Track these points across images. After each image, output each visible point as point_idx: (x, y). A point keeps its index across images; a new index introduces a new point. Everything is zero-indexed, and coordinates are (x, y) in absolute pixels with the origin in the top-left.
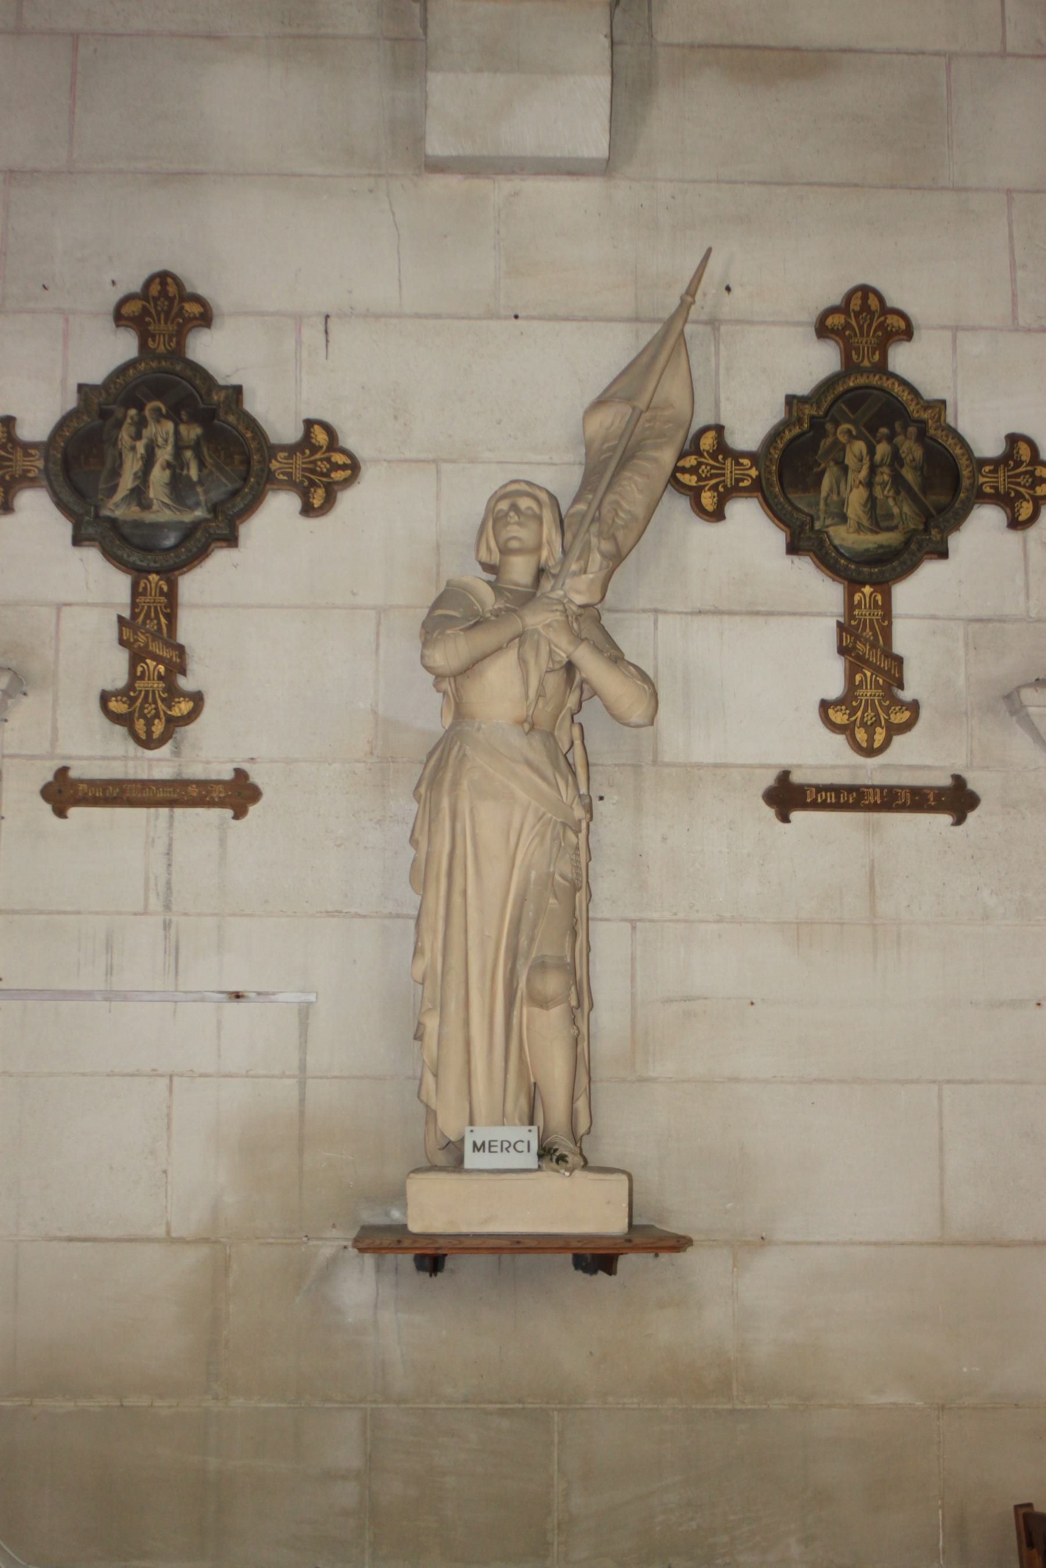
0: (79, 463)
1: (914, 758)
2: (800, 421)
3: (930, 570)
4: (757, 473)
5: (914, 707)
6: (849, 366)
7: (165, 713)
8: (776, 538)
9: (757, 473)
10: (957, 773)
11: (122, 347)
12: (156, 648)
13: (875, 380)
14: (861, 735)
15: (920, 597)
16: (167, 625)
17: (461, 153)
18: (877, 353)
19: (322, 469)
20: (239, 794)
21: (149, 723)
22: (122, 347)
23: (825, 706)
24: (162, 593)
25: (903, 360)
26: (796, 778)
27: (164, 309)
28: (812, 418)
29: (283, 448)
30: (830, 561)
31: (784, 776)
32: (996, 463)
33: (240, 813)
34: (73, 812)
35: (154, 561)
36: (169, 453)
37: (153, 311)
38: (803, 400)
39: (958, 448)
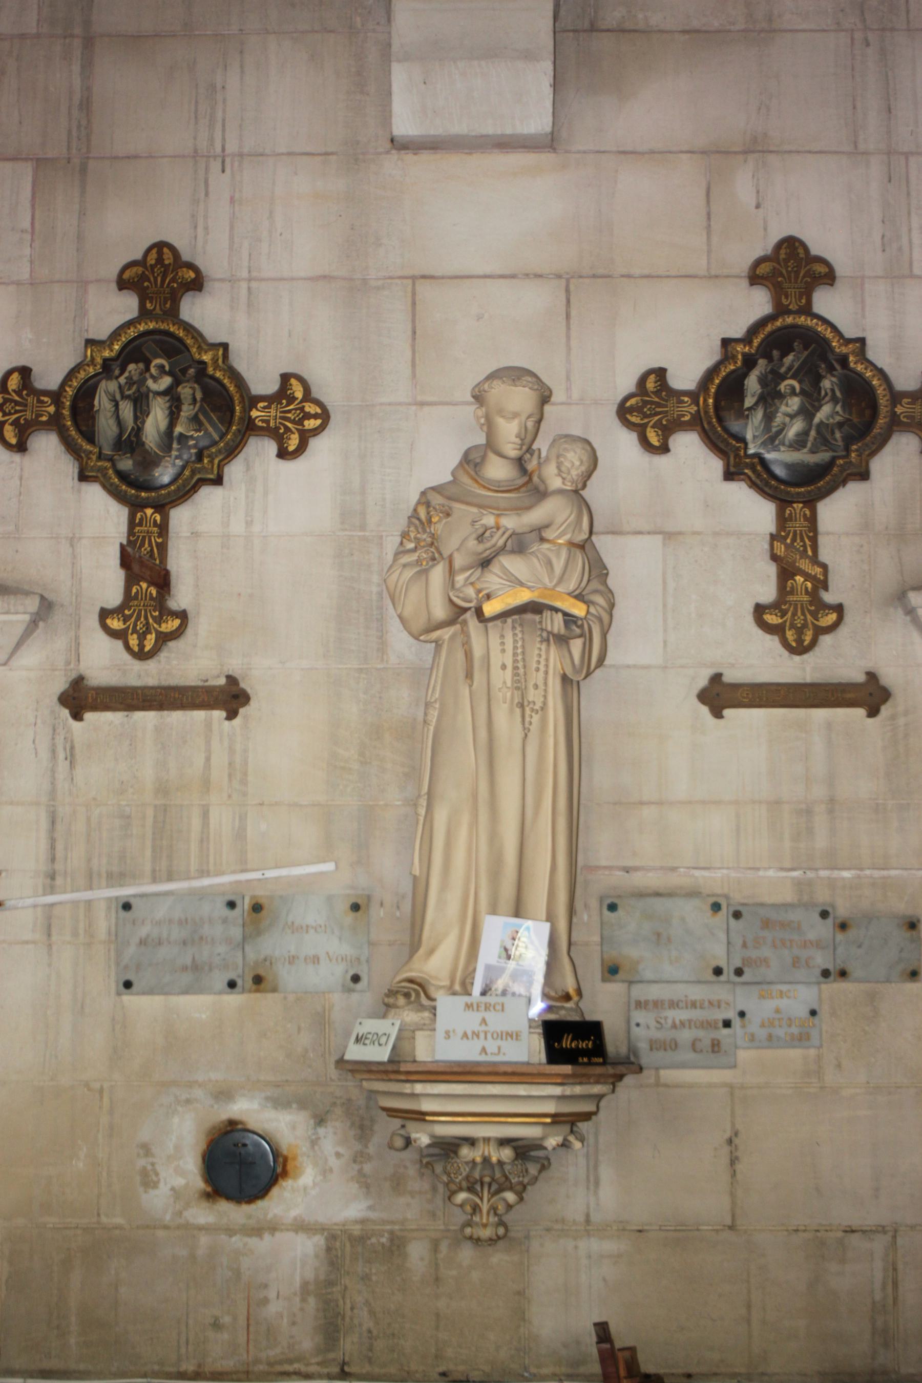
0: (72, 413)
1: (836, 658)
2: (734, 357)
4: (252, 413)
5: (839, 609)
6: (780, 310)
7: (813, 623)
9: (252, 413)
10: (230, 673)
11: (758, 304)
12: (804, 565)
13: (802, 320)
14: (310, 424)
15: (838, 512)
16: (159, 553)
19: (294, 417)
20: (231, 698)
22: (758, 304)
23: (759, 610)
26: (728, 678)
27: (162, 277)
28: (744, 355)
29: (262, 398)
30: (761, 478)
31: (716, 678)
32: (271, 399)
33: (232, 715)
34: (89, 716)
35: (146, 494)
36: (161, 404)
37: (784, 272)
39: (876, 379)
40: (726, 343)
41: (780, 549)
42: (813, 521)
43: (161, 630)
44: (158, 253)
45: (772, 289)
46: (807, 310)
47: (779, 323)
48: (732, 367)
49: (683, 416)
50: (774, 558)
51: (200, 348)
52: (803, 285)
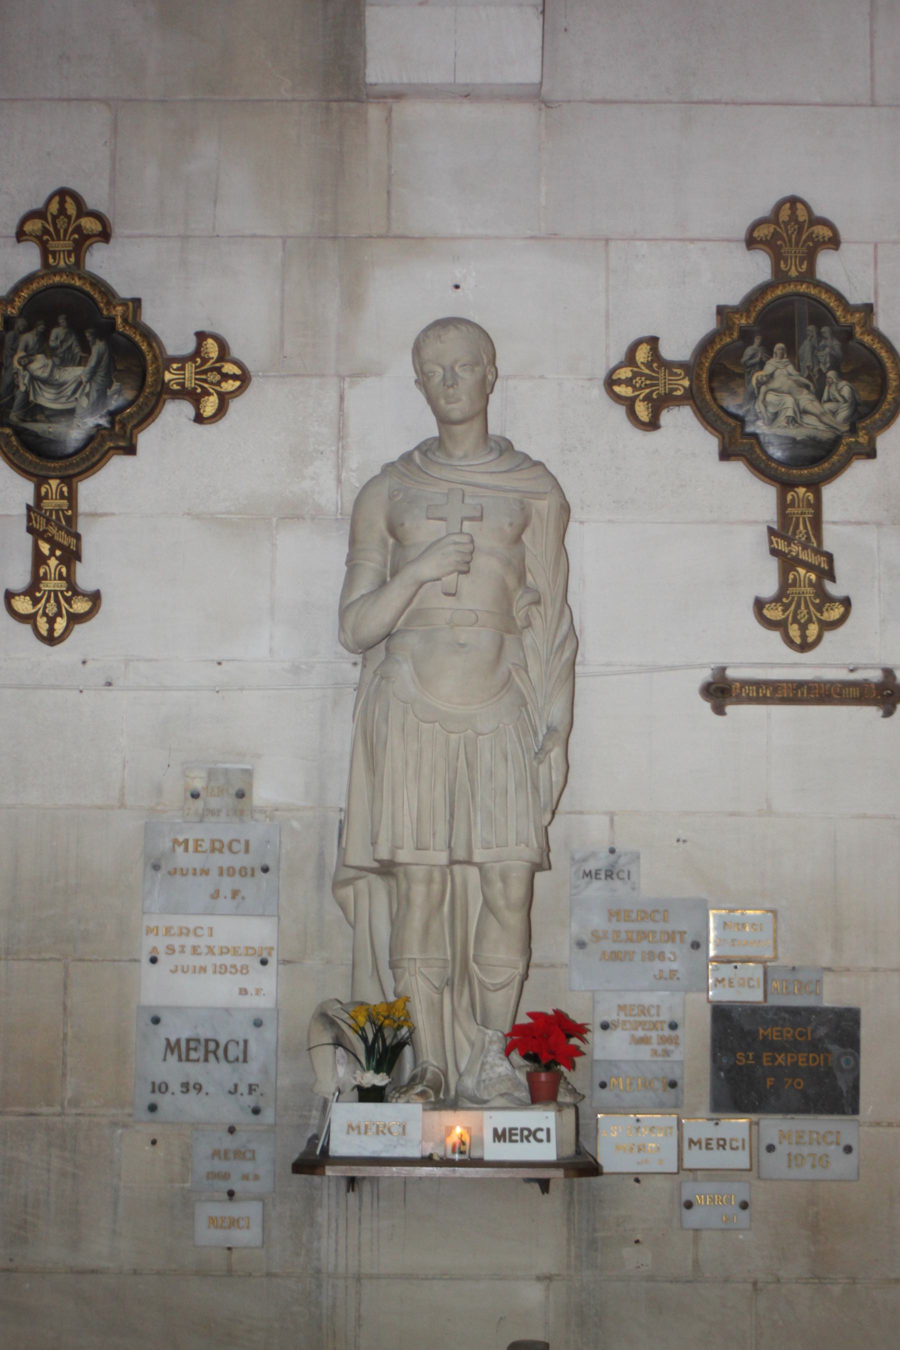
3: (859, 469)
6: (779, 276)
8: (708, 443)
11: (757, 269)
13: (803, 288)
14: (794, 631)
17: (396, 80)
18: (805, 263)
21: (803, 628)
22: (757, 269)
24: (809, 505)
25: (829, 268)
29: (174, 360)
30: (762, 467)
38: (736, 310)
40: (721, 311)
41: (781, 546)
42: (817, 506)
43: (823, 618)
44: (791, 208)
45: (769, 251)
46: (809, 276)
47: (779, 292)
48: (728, 340)
49: (676, 389)
50: (774, 552)
51: (109, 304)
52: (70, 242)
